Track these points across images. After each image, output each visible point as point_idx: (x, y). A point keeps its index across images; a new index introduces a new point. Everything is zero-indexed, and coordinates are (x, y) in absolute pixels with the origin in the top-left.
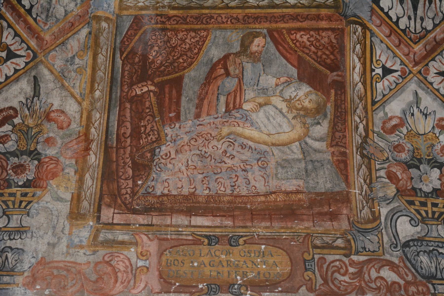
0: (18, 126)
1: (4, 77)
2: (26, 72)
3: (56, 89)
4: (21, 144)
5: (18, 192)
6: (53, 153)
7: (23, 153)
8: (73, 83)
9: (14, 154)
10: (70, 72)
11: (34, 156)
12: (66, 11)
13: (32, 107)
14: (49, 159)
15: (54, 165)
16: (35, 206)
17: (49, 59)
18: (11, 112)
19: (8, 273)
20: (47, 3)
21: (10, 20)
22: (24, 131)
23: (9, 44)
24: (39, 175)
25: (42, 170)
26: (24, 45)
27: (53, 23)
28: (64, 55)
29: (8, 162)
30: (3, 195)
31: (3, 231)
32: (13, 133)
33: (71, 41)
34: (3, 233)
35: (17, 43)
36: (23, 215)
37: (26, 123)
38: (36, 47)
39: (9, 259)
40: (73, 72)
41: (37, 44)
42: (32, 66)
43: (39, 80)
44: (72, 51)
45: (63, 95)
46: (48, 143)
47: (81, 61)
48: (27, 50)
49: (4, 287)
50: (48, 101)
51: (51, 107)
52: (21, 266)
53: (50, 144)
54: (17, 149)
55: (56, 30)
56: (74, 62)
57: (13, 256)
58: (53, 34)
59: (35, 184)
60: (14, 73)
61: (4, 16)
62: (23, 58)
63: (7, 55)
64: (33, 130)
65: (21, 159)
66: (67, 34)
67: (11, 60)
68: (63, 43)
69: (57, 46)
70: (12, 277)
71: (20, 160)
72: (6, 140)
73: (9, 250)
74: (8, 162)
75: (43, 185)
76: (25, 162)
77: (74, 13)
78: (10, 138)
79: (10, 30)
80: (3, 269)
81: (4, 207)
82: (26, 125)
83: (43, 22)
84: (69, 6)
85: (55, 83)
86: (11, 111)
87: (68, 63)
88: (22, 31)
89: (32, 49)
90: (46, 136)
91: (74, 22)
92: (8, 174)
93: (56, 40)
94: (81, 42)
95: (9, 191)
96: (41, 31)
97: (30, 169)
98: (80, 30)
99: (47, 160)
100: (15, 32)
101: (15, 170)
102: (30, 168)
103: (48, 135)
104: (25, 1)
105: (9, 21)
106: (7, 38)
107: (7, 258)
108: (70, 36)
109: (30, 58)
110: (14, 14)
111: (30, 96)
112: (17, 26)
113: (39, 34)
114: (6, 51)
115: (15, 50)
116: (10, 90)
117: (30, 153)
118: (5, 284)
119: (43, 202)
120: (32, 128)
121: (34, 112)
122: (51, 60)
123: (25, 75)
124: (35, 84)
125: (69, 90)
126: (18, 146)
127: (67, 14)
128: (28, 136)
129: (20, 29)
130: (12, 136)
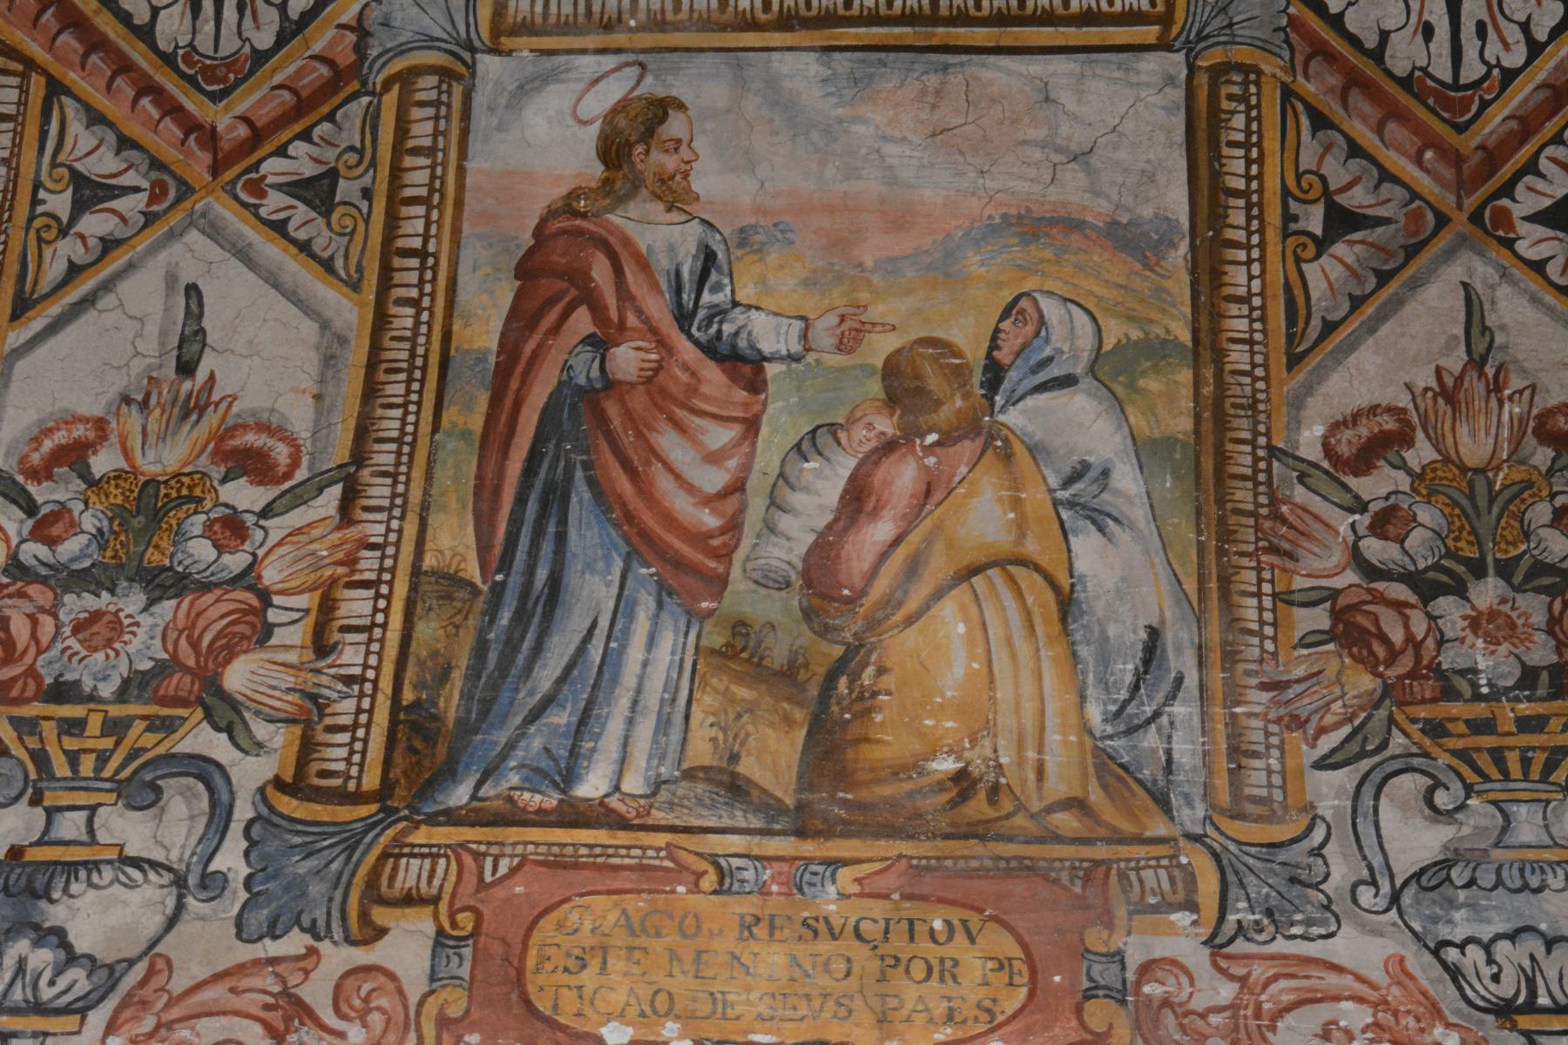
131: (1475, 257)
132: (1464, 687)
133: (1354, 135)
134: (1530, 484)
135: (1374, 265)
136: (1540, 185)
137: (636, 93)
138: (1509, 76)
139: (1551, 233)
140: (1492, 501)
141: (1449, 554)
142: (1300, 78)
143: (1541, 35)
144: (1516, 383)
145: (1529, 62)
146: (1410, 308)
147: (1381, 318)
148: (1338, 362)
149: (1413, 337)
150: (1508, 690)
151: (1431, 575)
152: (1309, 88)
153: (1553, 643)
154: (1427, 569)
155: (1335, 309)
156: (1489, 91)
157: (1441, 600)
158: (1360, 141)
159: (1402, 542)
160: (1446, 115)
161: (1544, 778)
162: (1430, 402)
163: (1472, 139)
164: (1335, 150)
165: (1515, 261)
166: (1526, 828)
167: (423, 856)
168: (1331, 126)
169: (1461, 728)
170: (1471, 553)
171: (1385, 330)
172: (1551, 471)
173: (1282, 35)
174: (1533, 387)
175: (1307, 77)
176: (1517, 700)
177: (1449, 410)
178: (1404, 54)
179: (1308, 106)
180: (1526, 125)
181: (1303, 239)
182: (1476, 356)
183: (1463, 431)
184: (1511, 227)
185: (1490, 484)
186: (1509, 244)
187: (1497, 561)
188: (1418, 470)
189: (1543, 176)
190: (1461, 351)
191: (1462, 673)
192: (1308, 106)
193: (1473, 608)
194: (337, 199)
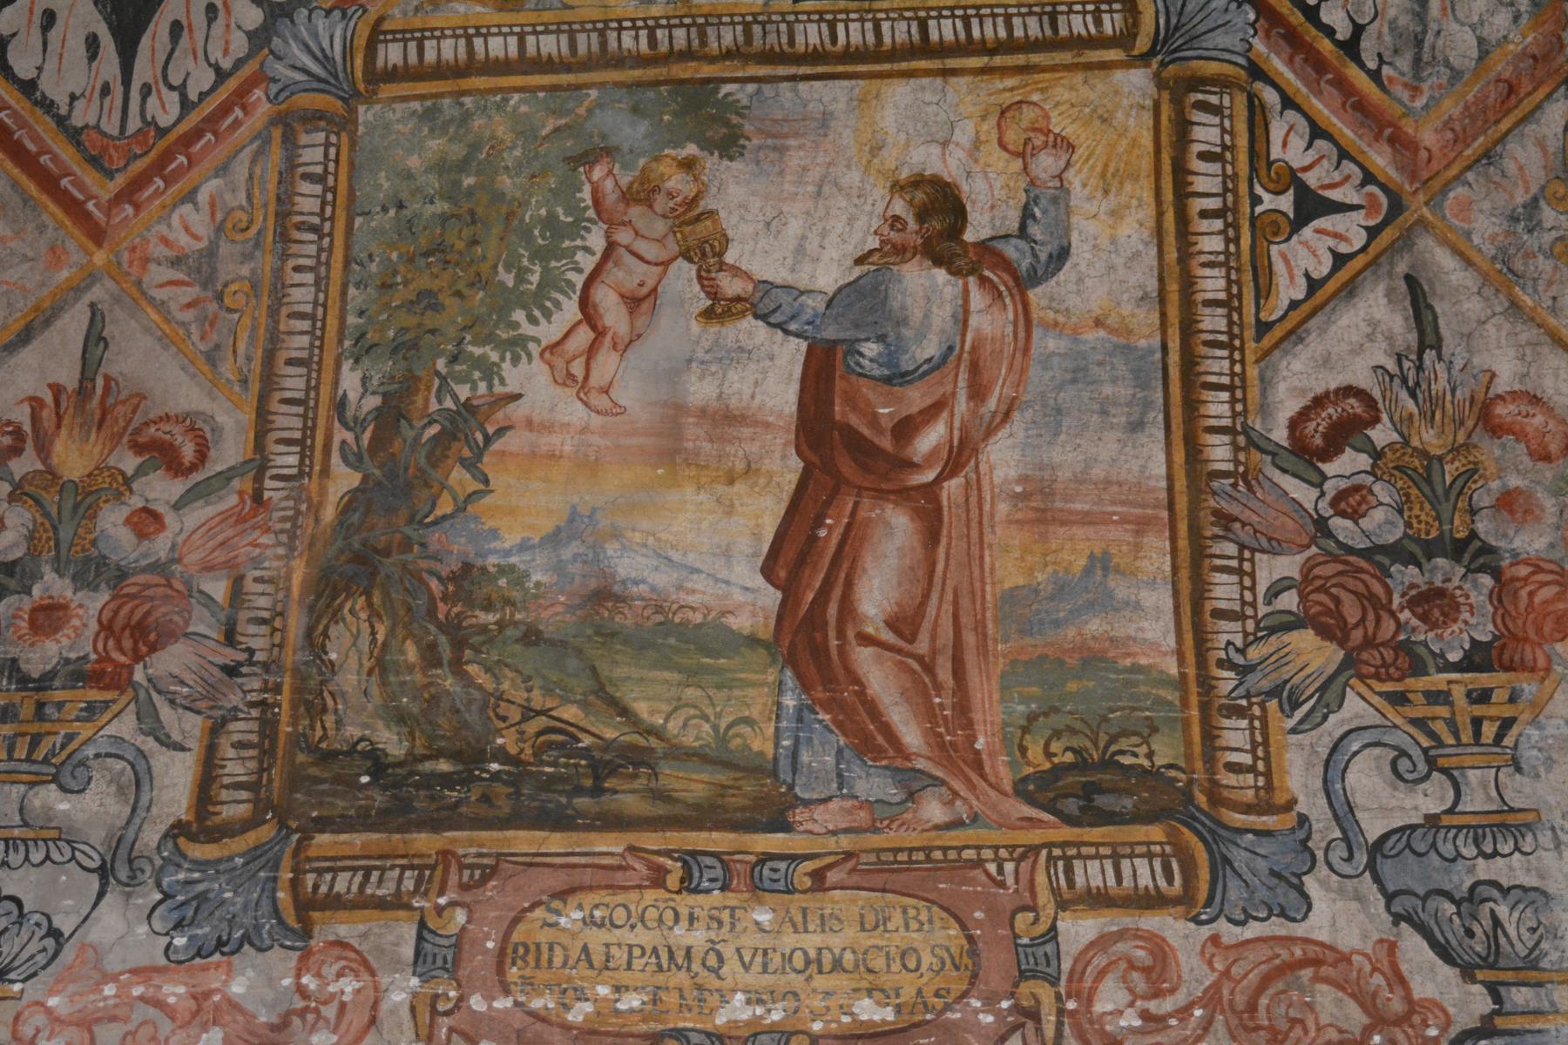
0: (1389, 455)
1: (1302, 283)
2: (1374, 263)
3: (1493, 320)
4: (1417, 517)
5: (1453, 686)
6: (1537, 546)
7: (1431, 549)
8: (1550, 294)
9: (1398, 553)
10: (1529, 255)
11: (1474, 558)
12: (1481, 41)
13: (1424, 386)
14: (1530, 569)
15: (1555, 589)
16: (1529, 737)
17: (1447, 212)
18: (1354, 406)
19: (1522, 975)
20: (1410, 17)
21: (1289, 83)
22: (1415, 470)
23: (1295, 165)
24: (1511, 626)
25: (1516, 607)
26: (1349, 167)
27: (1440, 86)
28: (1500, 198)
29: (1388, 581)
30: (1409, 701)
31: (1449, 828)
32: (1377, 479)
33: (1512, 146)
34: (1451, 835)
35: (1325, 162)
36: (1498, 768)
37: (1415, 443)
38: (1392, 173)
39: (1507, 925)
40: (1541, 258)
41: (1395, 162)
42: (1393, 243)
43: (1426, 288)
44: (1526, 182)
45: (1524, 337)
46: (1512, 512)
47: (1562, 218)
48: (1363, 184)
49: (1527, 1027)
50: (1476, 361)
51: (1490, 382)
52: (1556, 949)
53: (1519, 515)
54: (1406, 535)
55: (1456, 111)
56: (1539, 223)
57: (1516, 915)
58: (1447, 124)
59: (1506, 657)
60: (1335, 269)
61: (1265, 67)
62: (1354, 214)
63: (1298, 204)
64: (1447, 468)
65: (1432, 571)
66: (1497, 122)
67: (1317, 223)
68: (1487, 156)
69: (1469, 168)
70: (1542, 991)
71: (1427, 575)
72: (1359, 504)
73: (1495, 893)
74: (1388, 581)
75: (1535, 660)
76: (1449, 580)
77: (1511, 47)
78: (1370, 498)
79: (1291, 115)
80: (1496, 961)
81: (1425, 743)
82: (1415, 449)
83: (1406, 85)
84: (1491, 24)
85: (1487, 299)
86: (1352, 401)
87: (1520, 227)
88: (1334, 120)
89: (1382, 179)
90: (1495, 485)
91: (1515, 82)
92: (1399, 626)
93: (1460, 146)
94: (1551, 150)
95: (1421, 683)
96: (1405, 115)
97: (1471, 606)
98: (1539, 107)
99: (1523, 571)
100: (1312, 123)
101: (1420, 610)
102: (1472, 600)
103: (1504, 485)
104: (1333, 16)
105: (1284, 86)
106: (1285, 144)
107: (1496, 922)
108: (1509, 131)
109: (1378, 212)
110: (1298, 59)
111: (1408, 348)
112: (1315, 101)
113: (1397, 128)
114: (1291, 191)
115: (1325, 187)
116: (1334, 328)
117: (1457, 549)
118: (1523, 1013)
119: (1553, 721)
120: (1440, 459)
121: (1435, 402)
122: (1456, 216)
123: (1375, 273)
124: (1415, 304)
125: (1538, 320)
126: (1408, 525)
127: (1487, 52)
128: (1433, 491)
129: (1326, 112)
130: (1377, 488)
137: (972, 463)
167: (355, 869)
169: (1420, 699)
194: (1367, 874)
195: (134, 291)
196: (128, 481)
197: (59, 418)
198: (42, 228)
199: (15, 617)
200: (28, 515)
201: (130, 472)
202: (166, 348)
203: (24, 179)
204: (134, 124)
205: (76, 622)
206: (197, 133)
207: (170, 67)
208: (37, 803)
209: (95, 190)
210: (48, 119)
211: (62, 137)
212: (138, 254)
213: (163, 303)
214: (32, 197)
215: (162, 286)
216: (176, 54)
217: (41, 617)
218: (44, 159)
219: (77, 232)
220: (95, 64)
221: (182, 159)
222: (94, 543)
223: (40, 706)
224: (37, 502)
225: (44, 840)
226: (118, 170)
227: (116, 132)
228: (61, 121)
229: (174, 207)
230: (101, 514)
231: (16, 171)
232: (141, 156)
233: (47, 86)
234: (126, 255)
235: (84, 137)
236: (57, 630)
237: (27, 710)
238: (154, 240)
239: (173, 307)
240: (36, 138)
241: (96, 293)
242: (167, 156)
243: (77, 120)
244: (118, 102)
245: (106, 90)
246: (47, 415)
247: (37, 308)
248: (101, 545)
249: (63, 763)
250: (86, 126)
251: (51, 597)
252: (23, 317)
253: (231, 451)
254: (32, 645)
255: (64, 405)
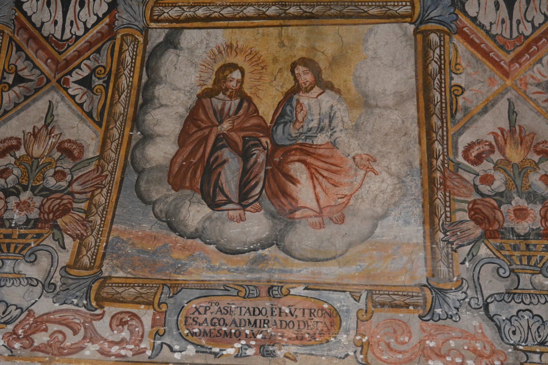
131: (55, 93)
132: (7, 224)
133: (28, 53)
134: (50, 163)
135: (24, 94)
136: (80, 72)
138: (78, 38)
139: (79, 87)
140: (37, 167)
141: (19, 184)
142: (16, 35)
143: (89, 26)
144: (57, 132)
145: (84, 34)
146: (32, 107)
147: (22, 110)
148: (5, 123)
149: (30, 117)
150: (20, 225)
151: (11, 189)
152: (18, 38)
153: (39, 212)
154: (11, 188)
155: (9, 107)
156: (71, 42)
157: (11, 197)
158: (30, 56)
159: (6, 179)
160: (57, 49)
161: (19, 253)
162: (29, 137)
163: (63, 57)
164: (21, 58)
165: (67, 95)
166: (7, 267)
168: (23, 51)
170: (25, 183)
171: (22, 114)
172: (58, 160)
173: (12, 21)
174: (61, 134)
175: (18, 35)
176: (22, 228)
177: (34, 139)
178: (48, 29)
179: (16, 44)
180: (80, 53)
181: (6, 85)
182: (47, 124)
183: (36, 146)
184: (68, 84)
185: (39, 162)
186: (66, 90)
187: (32, 186)
188: (18, 157)
189: (81, 69)
190: (43, 122)
191: (8, 220)
192: (16, 44)
193: (20, 200)
195: (524, 95)
196: (537, 164)
197: (505, 141)
198: (485, 71)
199: (508, 212)
200: (502, 175)
201: (537, 162)
202: (539, 116)
203: (475, 52)
204: (515, 34)
205: (531, 215)
206: (539, 39)
207: (527, 13)
208: (536, 281)
209: (504, 58)
210: (483, 31)
211: (488, 38)
212: (523, 82)
213: (535, 100)
214: (479, 59)
215: (534, 93)
216: (529, 9)
217: (518, 213)
218: (483, 46)
219: (498, 73)
220: (498, 12)
221: (535, 47)
222: (530, 186)
223: (527, 246)
224: (505, 171)
225: (544, 295)
226: (511, 51)
227: (509, 37)
228: (488, 32)
229: (534, 65)
230: (529, 176)
231: (472, 50)
232: (519, 46)
233: (481, 19)
234: (518, 82)
235: (497, 38)
236: (525, 218)
237: (523, 247)
238: (528, 77)
239: (540, 102)
240: (479, 38)
241: (509, 95)
242: (529, 47)
243: (494, 32)
244: (508, 26)
245: (503, 22)
246: (500, 138)
247: (487, 100)
248: (533, 187)
249: (542, 267)
250: (497, 34)
251: (519, 206)
252: (483, 103)
253: (92, 151)
254: (518, 223)
255: (506, 136)
